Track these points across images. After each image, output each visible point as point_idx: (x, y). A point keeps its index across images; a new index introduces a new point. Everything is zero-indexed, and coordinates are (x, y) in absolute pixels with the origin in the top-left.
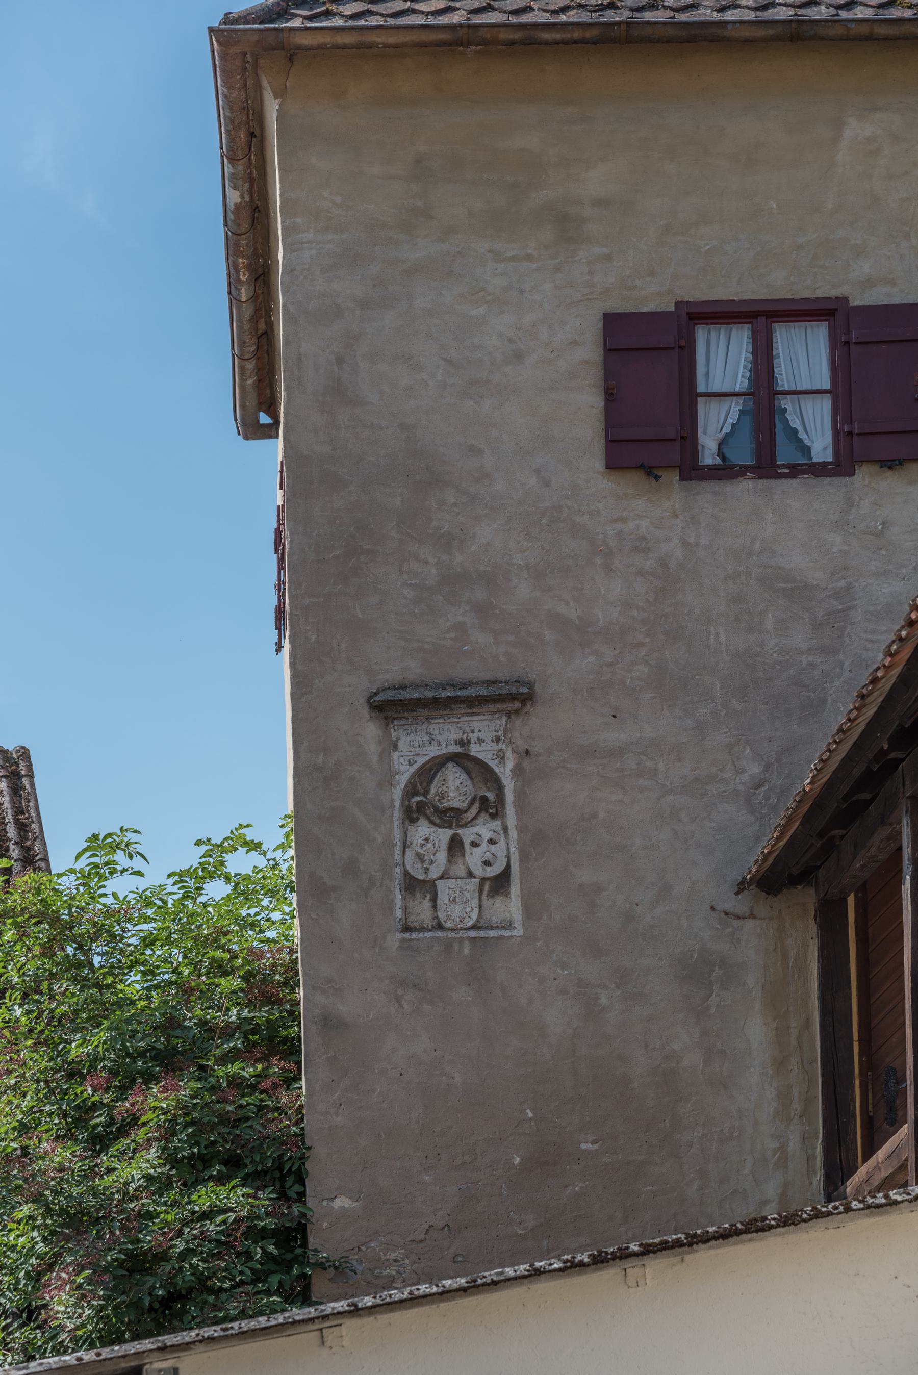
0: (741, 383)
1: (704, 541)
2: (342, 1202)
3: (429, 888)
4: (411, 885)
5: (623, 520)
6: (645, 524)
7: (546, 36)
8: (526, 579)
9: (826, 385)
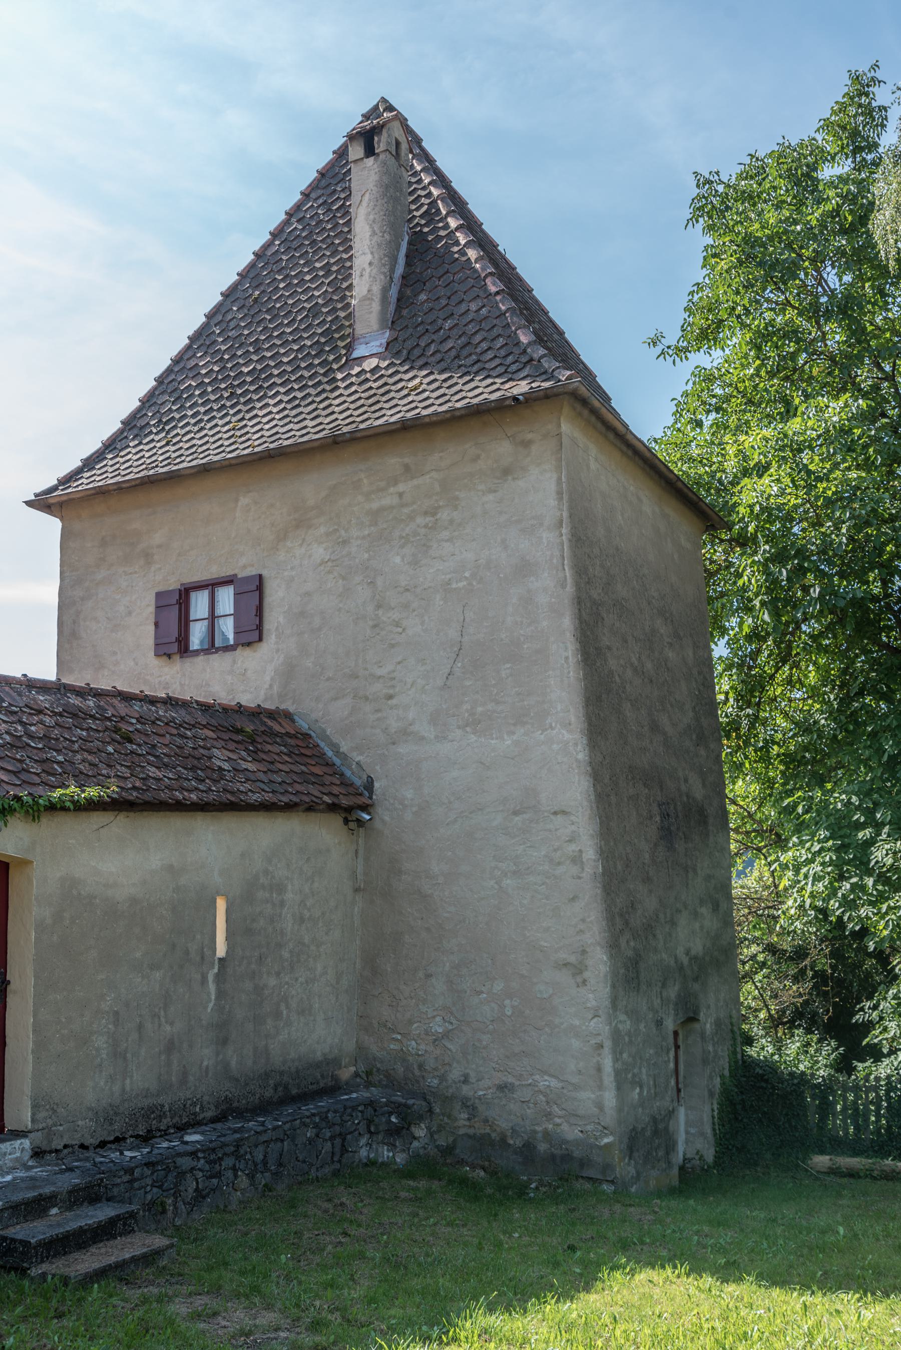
0: (206, 616)
1: (187, 683)
5: (160, 676)
6: (168, 677)
7: (124, 485)
8: (789, 518)
9: (232, 612)
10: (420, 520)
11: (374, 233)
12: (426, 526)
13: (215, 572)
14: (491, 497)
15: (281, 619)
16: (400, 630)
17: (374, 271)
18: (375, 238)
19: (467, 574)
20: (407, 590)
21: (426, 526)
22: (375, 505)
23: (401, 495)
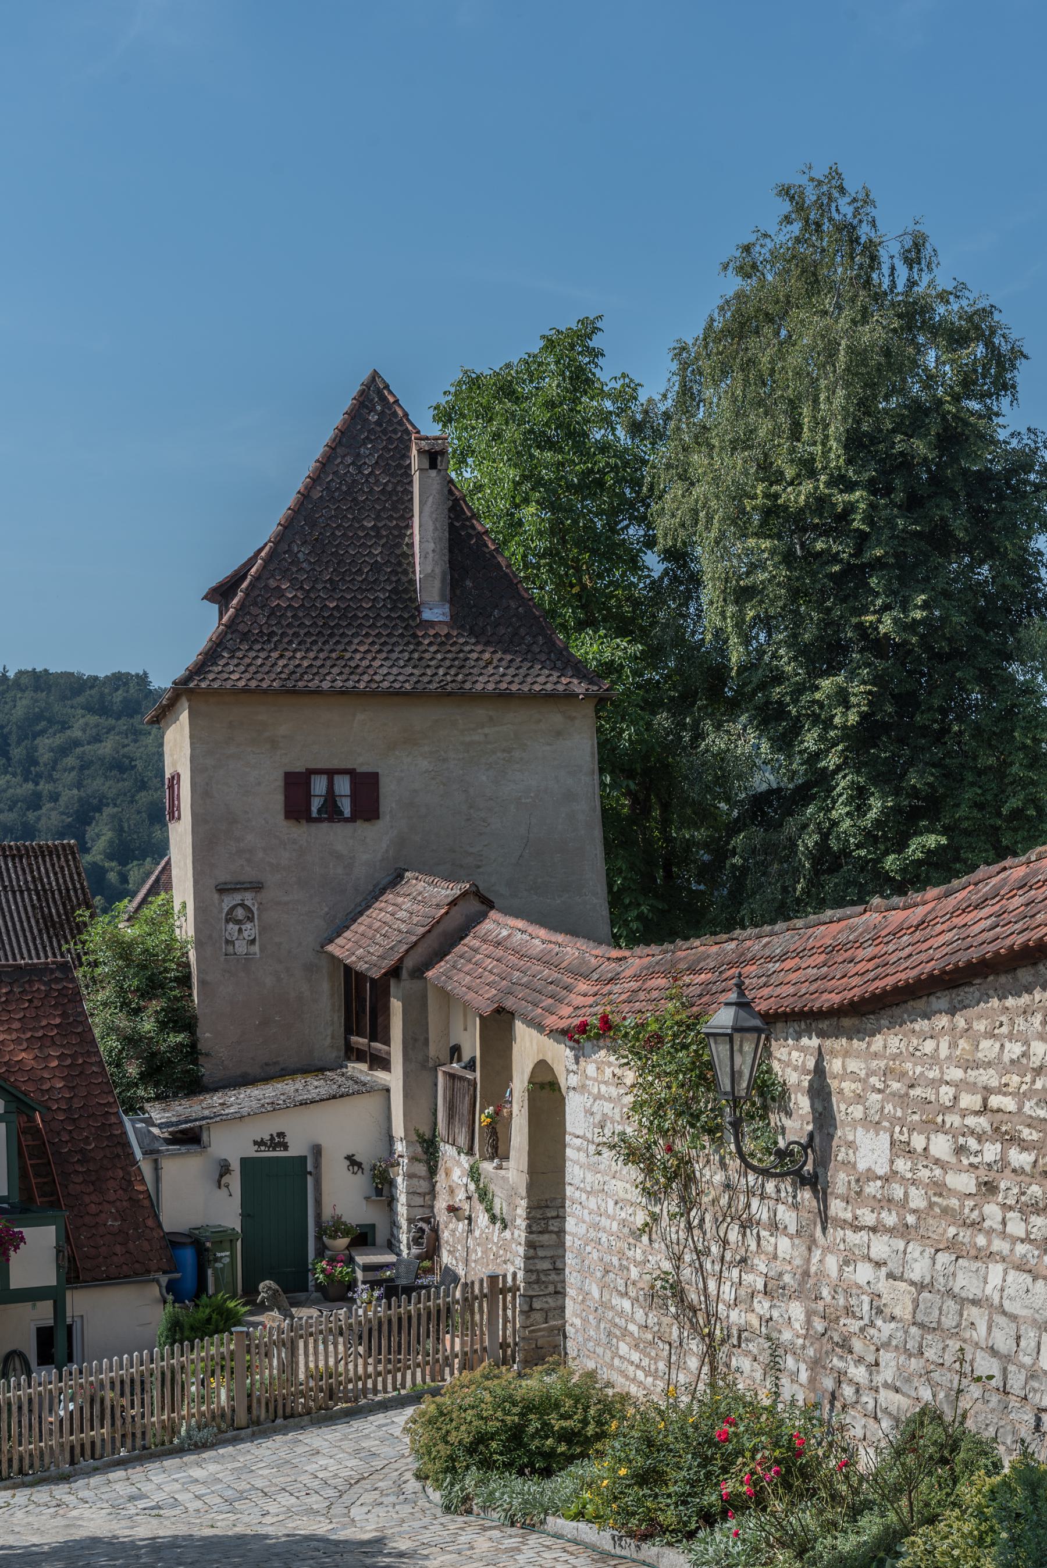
0: (324, 792)
2: (207, 1035)
3: (233, 943)
4: (227, 942)
10: (499, 754)
11: (436, 529)
13: (335, 764)
14: (548, 748)
22: (468, 739)
23: (486, 735)
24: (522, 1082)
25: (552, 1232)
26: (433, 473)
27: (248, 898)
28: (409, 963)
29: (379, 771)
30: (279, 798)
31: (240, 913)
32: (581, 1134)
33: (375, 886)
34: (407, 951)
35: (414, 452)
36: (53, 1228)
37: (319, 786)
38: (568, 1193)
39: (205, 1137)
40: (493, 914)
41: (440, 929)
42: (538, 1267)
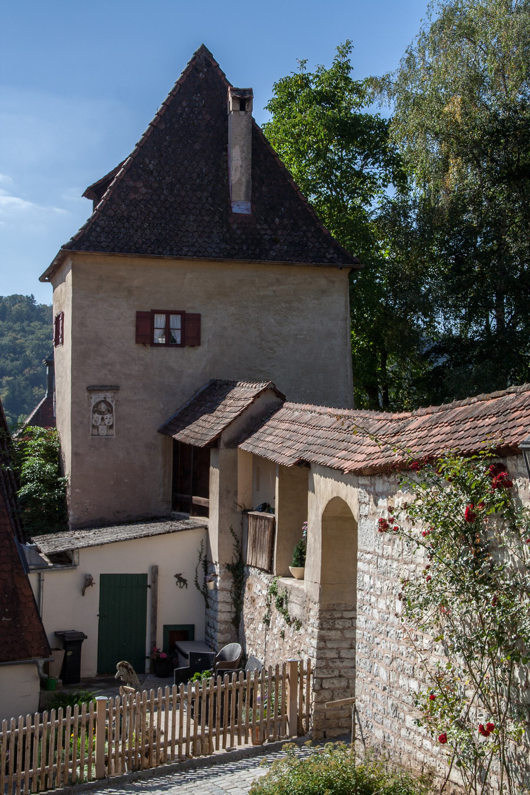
0: (163, 326)
4: (94, 426)
9: (180, 328)
12: (286, 308)
15: (210, 337)
16: (273, 352)
17: (243, 170)
18: (244, 154)
19: (305, 333)
20: (277, 335)
21: (286, 308)
23: (274, 291)
24: (316, 515)
25: (337, 629)
26: (242, 113)
27: (109, 396)
28: (225, 438)
29: (201, 313)
30: (132, 329)
31: (103, 407)
32: (371, 549)
33: (196, 391)
34: (224, 429)
35: (230, 99)
36: (92, 201)
37: (160, 321)
38: (359, 597)
39: (75, 558)
40: (286, 404)
41: (248, 413)
42: (327, 656)
